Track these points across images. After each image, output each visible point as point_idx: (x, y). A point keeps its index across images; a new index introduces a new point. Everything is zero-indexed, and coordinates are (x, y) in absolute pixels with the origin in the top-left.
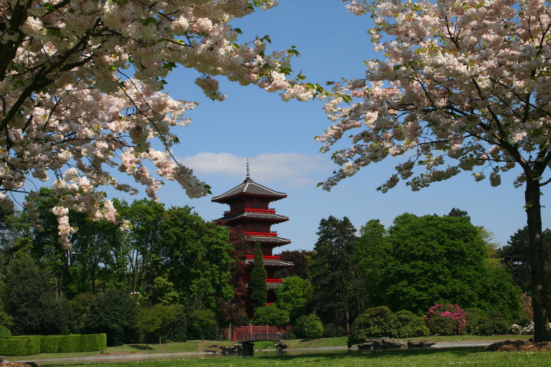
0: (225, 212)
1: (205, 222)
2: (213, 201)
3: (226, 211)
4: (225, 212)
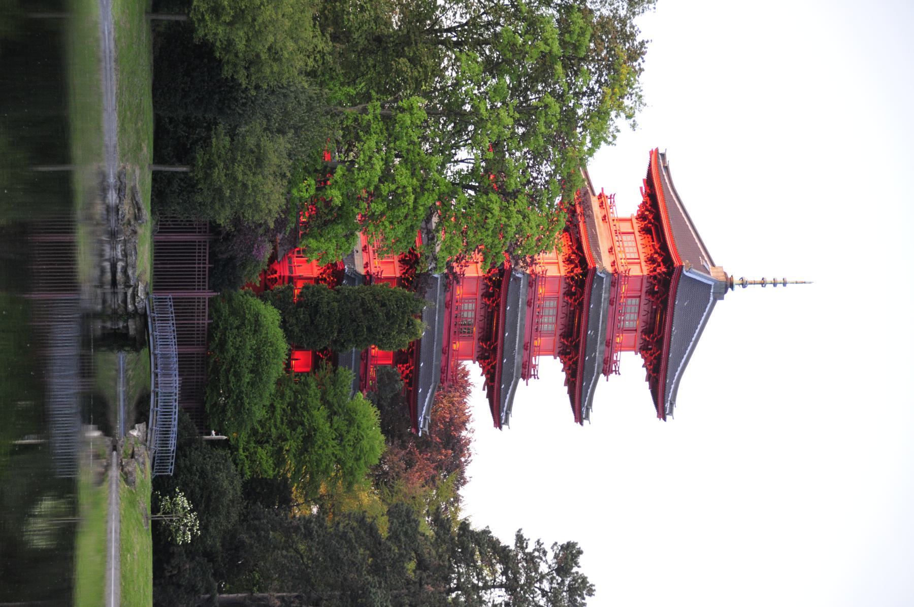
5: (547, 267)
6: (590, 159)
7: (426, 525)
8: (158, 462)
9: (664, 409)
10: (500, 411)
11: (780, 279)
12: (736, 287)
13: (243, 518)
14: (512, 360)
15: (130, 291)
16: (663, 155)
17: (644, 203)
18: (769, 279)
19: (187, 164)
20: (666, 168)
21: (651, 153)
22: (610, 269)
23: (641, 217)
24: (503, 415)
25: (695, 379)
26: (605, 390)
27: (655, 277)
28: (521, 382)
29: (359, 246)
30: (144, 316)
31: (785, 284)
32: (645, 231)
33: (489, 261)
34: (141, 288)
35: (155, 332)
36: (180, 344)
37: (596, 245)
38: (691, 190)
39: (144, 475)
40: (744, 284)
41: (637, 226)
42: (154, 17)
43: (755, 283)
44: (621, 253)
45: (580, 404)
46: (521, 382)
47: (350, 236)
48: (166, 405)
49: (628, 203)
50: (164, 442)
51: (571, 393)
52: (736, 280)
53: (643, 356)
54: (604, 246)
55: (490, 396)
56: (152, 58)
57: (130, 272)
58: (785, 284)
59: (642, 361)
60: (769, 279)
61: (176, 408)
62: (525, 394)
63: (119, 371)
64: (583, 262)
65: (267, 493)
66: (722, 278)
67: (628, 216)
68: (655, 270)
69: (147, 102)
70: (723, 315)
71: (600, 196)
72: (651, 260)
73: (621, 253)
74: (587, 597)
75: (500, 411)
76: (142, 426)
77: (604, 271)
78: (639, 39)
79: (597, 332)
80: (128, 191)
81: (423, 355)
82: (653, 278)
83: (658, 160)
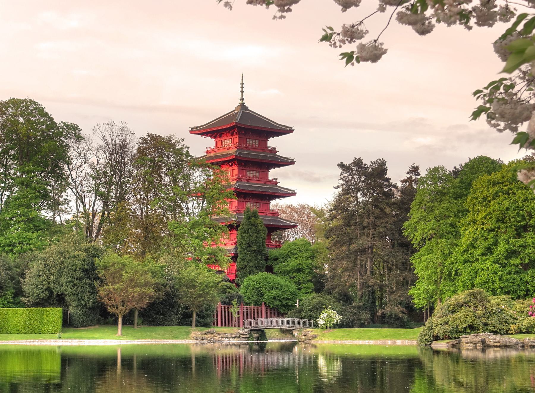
0: (207, 148)
1: (134, 147)
5: (234, 174)
8: (307, 325)
9: (290, 130)
10: (291, 193)
11: (241, 86)
12: (244, 102)
13: (330, 293)
14: (270, 188)
15: (242, 336)
16: (192, 129)
17: (211, 136)
18: (240, 89)
19: (192, 314)
20: (197, 127)
21: (191, 133)
22: (236, 150)
23: (215, 137)
24: (291, 192)
26: (281, 152)
27: (239, 133)
28: (278, 185)
29: (225, 247)
30: (251, 330)
31: (242, 84)
32: (221, 136)
33: (232, 196)
34: (241, 332)
35: (256, 326)
36: (260, 317)
37: (226, 155)
38: (202, 121)
39: (313, 332)
40: (242, 99)
41: (219, 139)
42: (136, 324)
43: (242, 95)
44: (230, 145)
45: (288, 162)
46: (278, 185)
47: (221, 251)
48: (289, 322)
49: (210, 142)
50: (300, 324)
51: (283, 166)
52: (240, 102)
54: (227, 152)
56: (97, 327)
57: (234, 336)
58: (242, 84)
60: (240, 89)
61: (286, 319)
63: (274, 340)
64: (233, 160)
66: (240, 107)
67: (215, 142)
68: (236, 133)
69: (169, 328)
70: (253, 107)
71: (207, 153)
72: (232, 134)
73: (230, 145)
74: (383, 47)
75: (291, 193)
76: (294, 332)
77: (236, 152)
79: (259, 155)
81: (268, 223)
82: (239, 133)
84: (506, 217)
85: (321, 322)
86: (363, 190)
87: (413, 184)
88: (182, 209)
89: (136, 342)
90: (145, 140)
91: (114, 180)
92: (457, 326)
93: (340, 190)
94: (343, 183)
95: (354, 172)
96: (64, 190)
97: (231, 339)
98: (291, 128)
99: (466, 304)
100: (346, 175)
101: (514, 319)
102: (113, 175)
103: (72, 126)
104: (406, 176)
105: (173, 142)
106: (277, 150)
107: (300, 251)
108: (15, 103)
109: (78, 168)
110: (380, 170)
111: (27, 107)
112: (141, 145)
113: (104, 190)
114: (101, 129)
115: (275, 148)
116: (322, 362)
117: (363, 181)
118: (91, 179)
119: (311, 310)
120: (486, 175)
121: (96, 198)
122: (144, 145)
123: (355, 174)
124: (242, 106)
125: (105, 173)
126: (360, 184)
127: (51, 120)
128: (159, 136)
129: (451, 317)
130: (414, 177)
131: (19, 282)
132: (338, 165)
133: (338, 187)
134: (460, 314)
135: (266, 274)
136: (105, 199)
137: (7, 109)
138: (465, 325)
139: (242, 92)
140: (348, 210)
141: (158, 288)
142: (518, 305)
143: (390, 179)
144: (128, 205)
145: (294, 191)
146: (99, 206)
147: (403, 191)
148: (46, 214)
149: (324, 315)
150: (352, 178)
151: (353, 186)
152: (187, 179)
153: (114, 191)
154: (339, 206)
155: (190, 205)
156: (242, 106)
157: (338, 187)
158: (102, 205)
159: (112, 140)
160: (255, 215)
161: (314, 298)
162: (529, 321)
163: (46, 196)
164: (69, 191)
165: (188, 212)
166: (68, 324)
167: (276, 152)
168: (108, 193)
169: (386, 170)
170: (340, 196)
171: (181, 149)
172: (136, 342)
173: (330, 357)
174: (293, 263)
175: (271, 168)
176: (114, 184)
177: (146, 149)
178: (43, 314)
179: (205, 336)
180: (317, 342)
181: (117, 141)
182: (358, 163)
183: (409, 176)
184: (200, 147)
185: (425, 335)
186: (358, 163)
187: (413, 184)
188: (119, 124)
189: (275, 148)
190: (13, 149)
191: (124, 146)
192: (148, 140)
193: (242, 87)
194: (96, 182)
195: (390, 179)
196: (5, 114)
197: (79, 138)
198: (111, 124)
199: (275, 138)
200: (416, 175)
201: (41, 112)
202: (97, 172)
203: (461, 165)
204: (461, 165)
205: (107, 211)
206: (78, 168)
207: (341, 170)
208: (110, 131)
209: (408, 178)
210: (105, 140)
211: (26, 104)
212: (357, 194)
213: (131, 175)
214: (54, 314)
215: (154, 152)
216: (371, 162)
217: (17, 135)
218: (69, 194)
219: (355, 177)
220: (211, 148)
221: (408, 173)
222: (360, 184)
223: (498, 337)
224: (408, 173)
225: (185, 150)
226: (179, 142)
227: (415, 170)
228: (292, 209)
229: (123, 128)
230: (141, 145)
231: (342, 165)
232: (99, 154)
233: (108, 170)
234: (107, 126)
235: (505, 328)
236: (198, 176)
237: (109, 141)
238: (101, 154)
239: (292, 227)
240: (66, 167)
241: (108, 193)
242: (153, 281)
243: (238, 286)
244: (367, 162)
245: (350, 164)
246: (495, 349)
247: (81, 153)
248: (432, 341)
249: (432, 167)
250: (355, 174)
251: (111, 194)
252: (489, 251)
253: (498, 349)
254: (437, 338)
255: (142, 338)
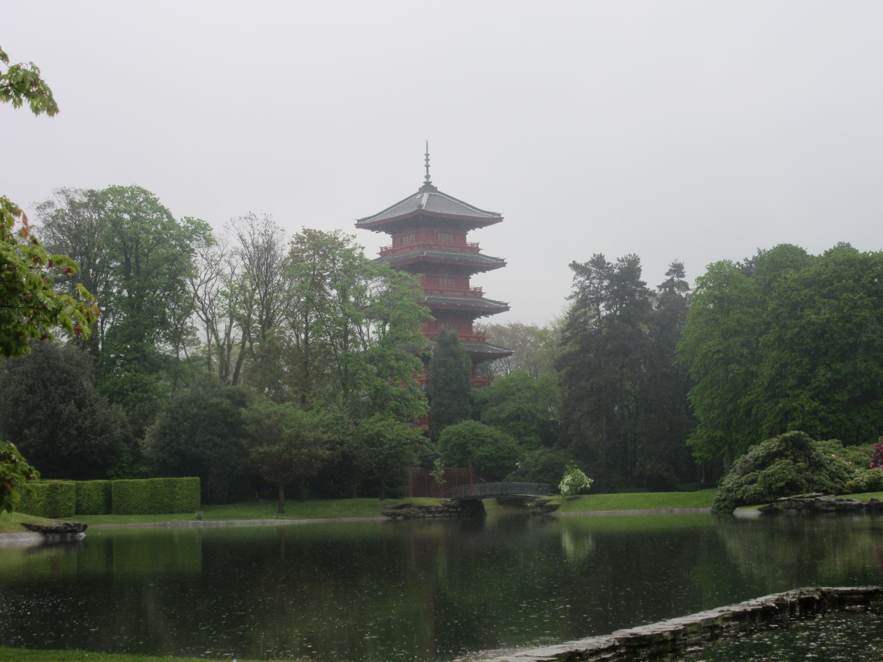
0: (381, 248)
1: (284, 249)
2: (358, 226)
3: (383, 245)
4: (381, 248)
6: (211, 232)
7: (567, 349)
10: (501, 308)
16: (359, 221)
18: (425, 163)
25: (479, 200)
38: (373, 208)
39: (554, 500)
40: (428, 177)
45: (496, 264)
49: (385, 240)
53: (813, 256)
55: (492, 314)
59: (471, 231)
62: (490, 294)
65: (549, 435)
69: (348, 502)
75: (501, 308)
78: (301, 233)
80: (395, 511)
83: (362, 224)
84: (826, 332)
85: (565, 488)
86: (608, 300)
87: (676, 289)
88: (353, 333)
89: (304, 521)
90: (300, 240)
91: (257, 297)
92: (770, 485)
93: (573, 301)
94: (578, 290)
95: (594, 275)
96: (188, 314)
97: (436, 515)
98: (499, 215)
99: (780, 454)
100: (582, 279)
101: (849, 472)
102: (255, 290)
103: (199, 223)
104: (665, 279)
105: (340, 239)
106: (480, 247)
107: (519, 390)
108: (117, 192)
109: (207, 281)
110: (631, 268)
111: (133, 197)
112: (295, 246)
113: (242, 312)
114: (236, 225)
115: (478, 244)
116: (567, 543)
117: (607, 288)
118: (223, 298)
119: (540, 472)
120: (791, 271)
121: (231, 322)
122: (299, 245)
123: (594, 278)
124: (428, 187)
125: (243, 288)
126: (603, 292)
127: (169, 216)
128: (320, 232)
129: (760, 474)
130: (676, 279)
131: (136, 444)
132: (570, 265)
133: (571, 297)
134: (773, 468)
135: (472, 423)
136: (246, 324)
137: (104, 202)
138: (782, 484)
139: (427, 166)
140: (585, 330)
141: (332, 445)
142: (855, 452)
143: (645, 284)
144: (280, 332)
145: (506, 304)
146: (237, 334)
147: (663, 301)
148: (165, 347)
149: (568, 478)
150: (591, 283)
151: (593, 294)
152: (361, 292)
153: (257, 313)
154: (574, 322)
155: (364, 329)
156: (428, 187)
157: (571, 297)
158: (241, 333)
159: (253, 241)
160: (454, 341)
161: (542, 454)
162: (871, 475)
163: (164, 323)
164: (194, 316)
165: (363, 339)
166: (210, 499)
167: (479, 250)
168: (249, 315)
169: (639, 270)
170: (575, 309)
171: (354, 249)
172: (304, 521)
173: (578, 534)
174: (510, 407)
175: (472, 273)
176: (256, 302)
177: (303, 251)
178: (175, 487)
179: (399, 511)
180: (560, 513)
181: (261, 241)
182: (598, 261)
183: (669, 278)
184: (374, 245)
185: (724, 500)
186: (598, 261)
187: (676, 289)
188: (261, 218)
189: (478, 244)
190: (116, 258)
191: (269, 247)
192: (304, 238)
193: (427, 160)
194: (230, 301)
195: (645, 284)
196: (103, 209)
197: (209, 242)
198: (251, 218)
199: (477, 230)
200: (678, 276)
201: (154, 205)
202: (232, 286)
203: (746, 260)
204: (746, 260)
205: (249, 341)
206: (207, 281)
207: (574, 273)
208: (249, 228)
209: (668, 281)
210: (243, 240)
211: (132, 193)
212: (598, 305)
213: (281, 290)
214: (189, 484)
215: (314, 255)
216: (619, 260)
217: (121, 237)
218: (195, 320)
219: (594, 281)
220: (386, 248)
221: (668, 274)
222: (603, 292)
223: (832, 498)
224: (668, 274)
225: (358, 251)
226: (348, 240)
227: (678, 269)
228: (498, 329)
229: (267, 223)
230: (295, 246)
231: (575, 266)
232: (234, 261)
233: (247, 283)
234: (245, 221)
235: (838, 486)
236: (375, 287)
237: (249, 241)
238: (237, 261)
239: (501, 356)
240: (188, 281)
241: (249, 315)
242: (325, 437)
243: (434, 440)
244: (611, 259)
245: (587, 264)
246: (830, 514)
247: (212, 260)
248: (734, 508)
249: (715, 261)
250: (594, 278)
251: (254, 317)
252: (803, 381)
253: (834, 514)
254: (742, 503)
255: (301, 515)
